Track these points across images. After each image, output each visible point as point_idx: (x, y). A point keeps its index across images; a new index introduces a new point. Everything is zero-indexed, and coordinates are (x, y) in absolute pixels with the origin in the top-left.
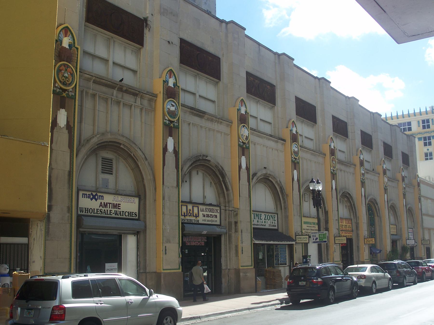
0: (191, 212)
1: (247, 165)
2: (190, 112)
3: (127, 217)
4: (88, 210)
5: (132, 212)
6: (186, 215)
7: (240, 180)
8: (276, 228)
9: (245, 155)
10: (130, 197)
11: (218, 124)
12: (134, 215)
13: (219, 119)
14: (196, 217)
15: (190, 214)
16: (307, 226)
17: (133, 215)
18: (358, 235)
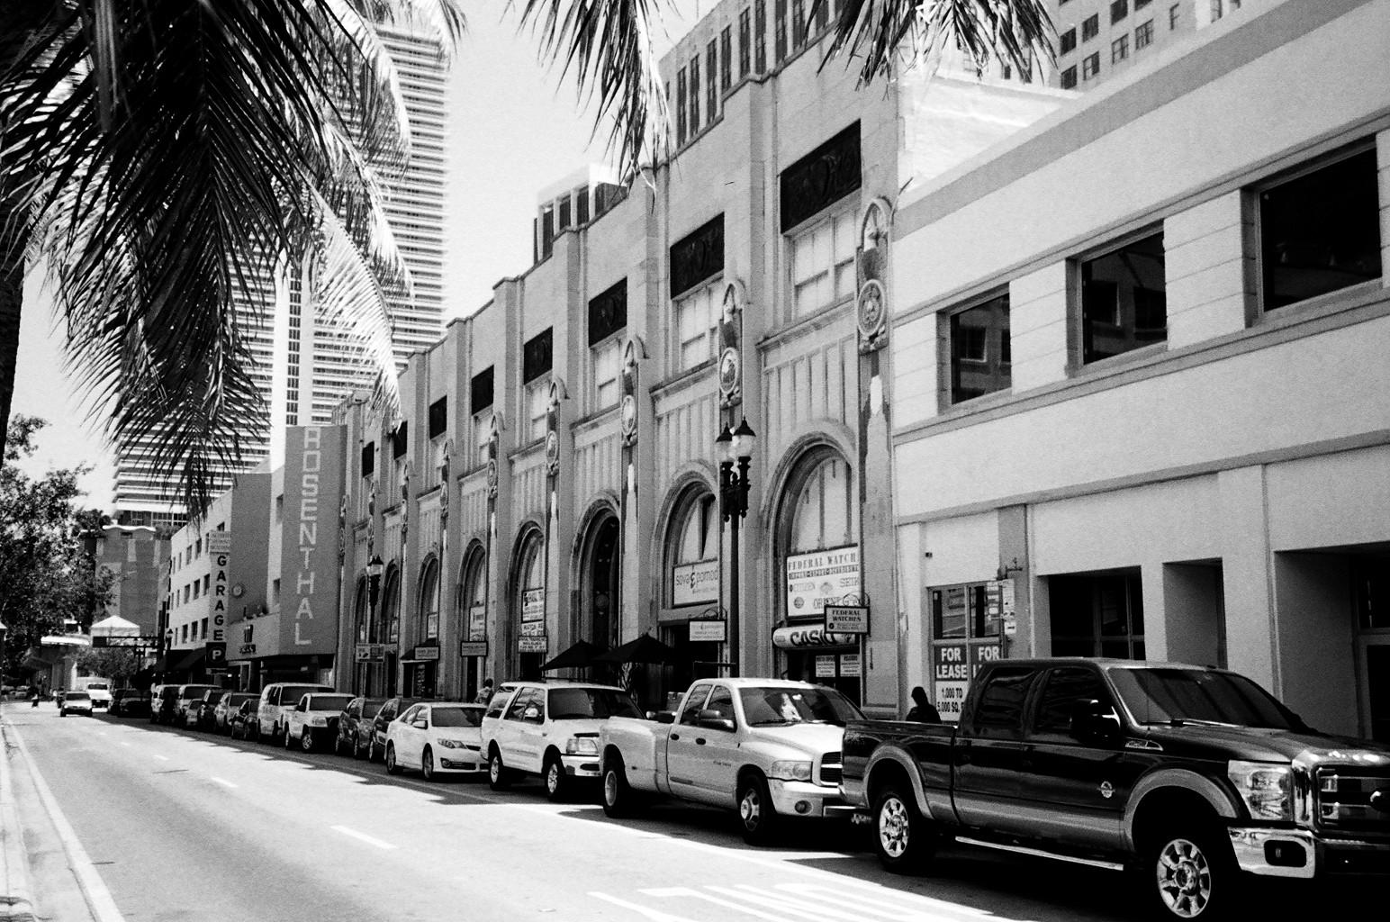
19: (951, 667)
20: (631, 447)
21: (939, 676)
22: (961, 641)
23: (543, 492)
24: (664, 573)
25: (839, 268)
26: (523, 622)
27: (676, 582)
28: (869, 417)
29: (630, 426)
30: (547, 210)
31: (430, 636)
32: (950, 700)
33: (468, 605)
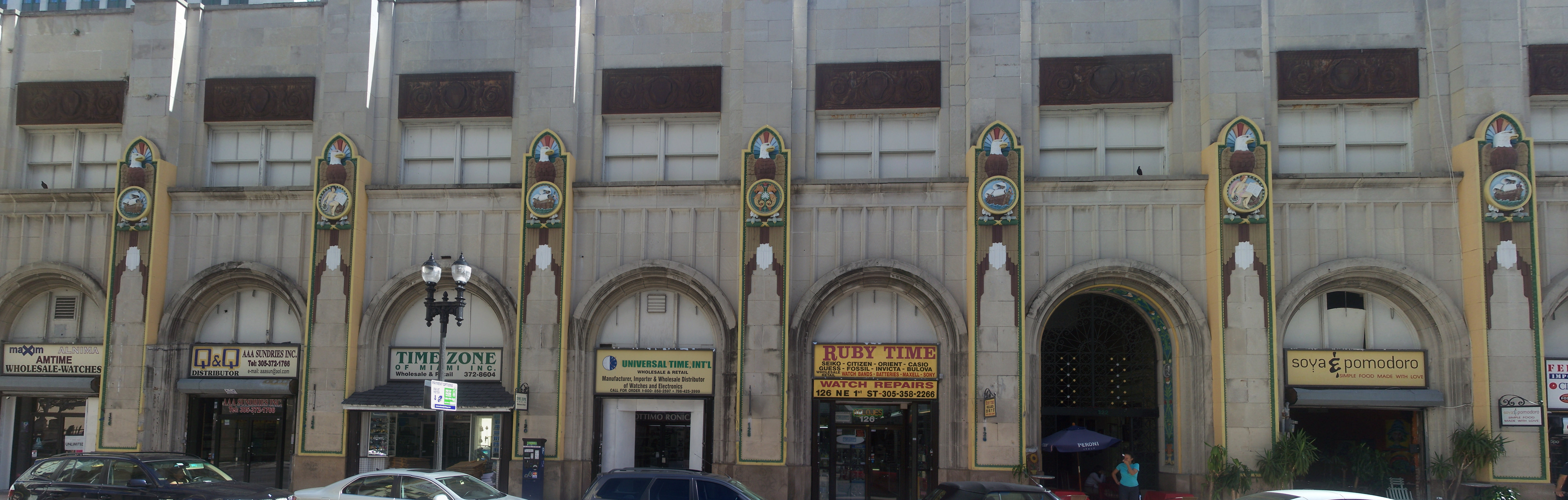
0: (220, 359)
2: (210, 197)
3: (84, 373)
4: (89, 369)
5: (93, 367)
6: (206, 363)
7: (118, 292)
8: (497, 378)
9: (339, 244)
10: (88, 346)
11: (289, 201)
12: (97, 370)
13: (281, 191)
14: (231, 366)
15: (215, 363)
16: (639, 372)
17: (94, 371)
18: (957, 392)
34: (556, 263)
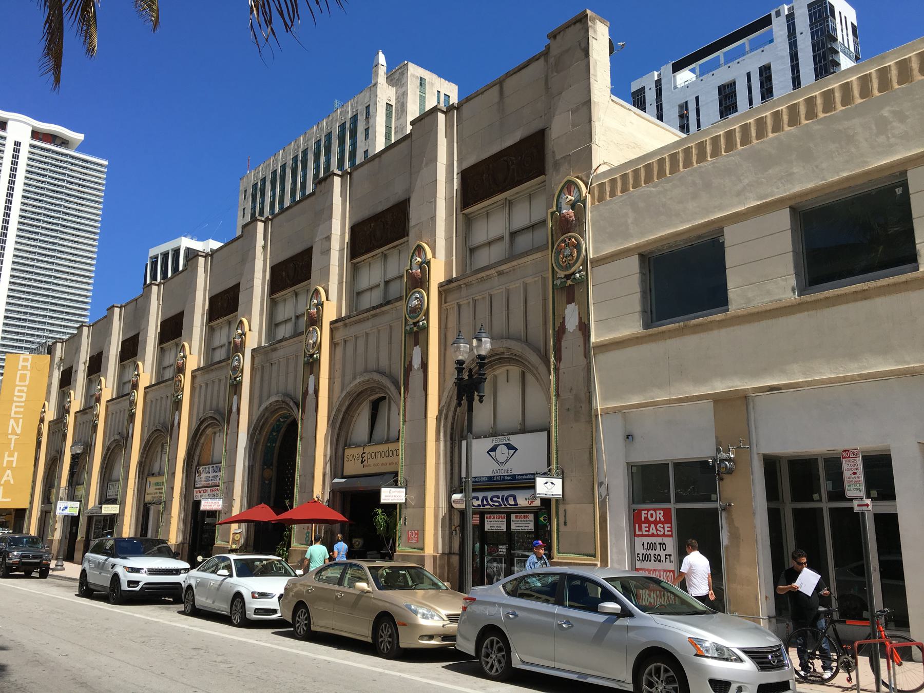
1: (422, 358)
19: (652, 526)
20: (178, 402)
21: (638, 532)
22: (666, 506)
23: (126, 421)
24: (336, 453)
25: (297, 317)
26: (195, 488)
27: (346, 459)
28: (411, 370)
29: (313, 348)
30: (154, 260)
31: (108, 497)
32: (652, 552)
33: (74, 483)
34: (583, 321)
